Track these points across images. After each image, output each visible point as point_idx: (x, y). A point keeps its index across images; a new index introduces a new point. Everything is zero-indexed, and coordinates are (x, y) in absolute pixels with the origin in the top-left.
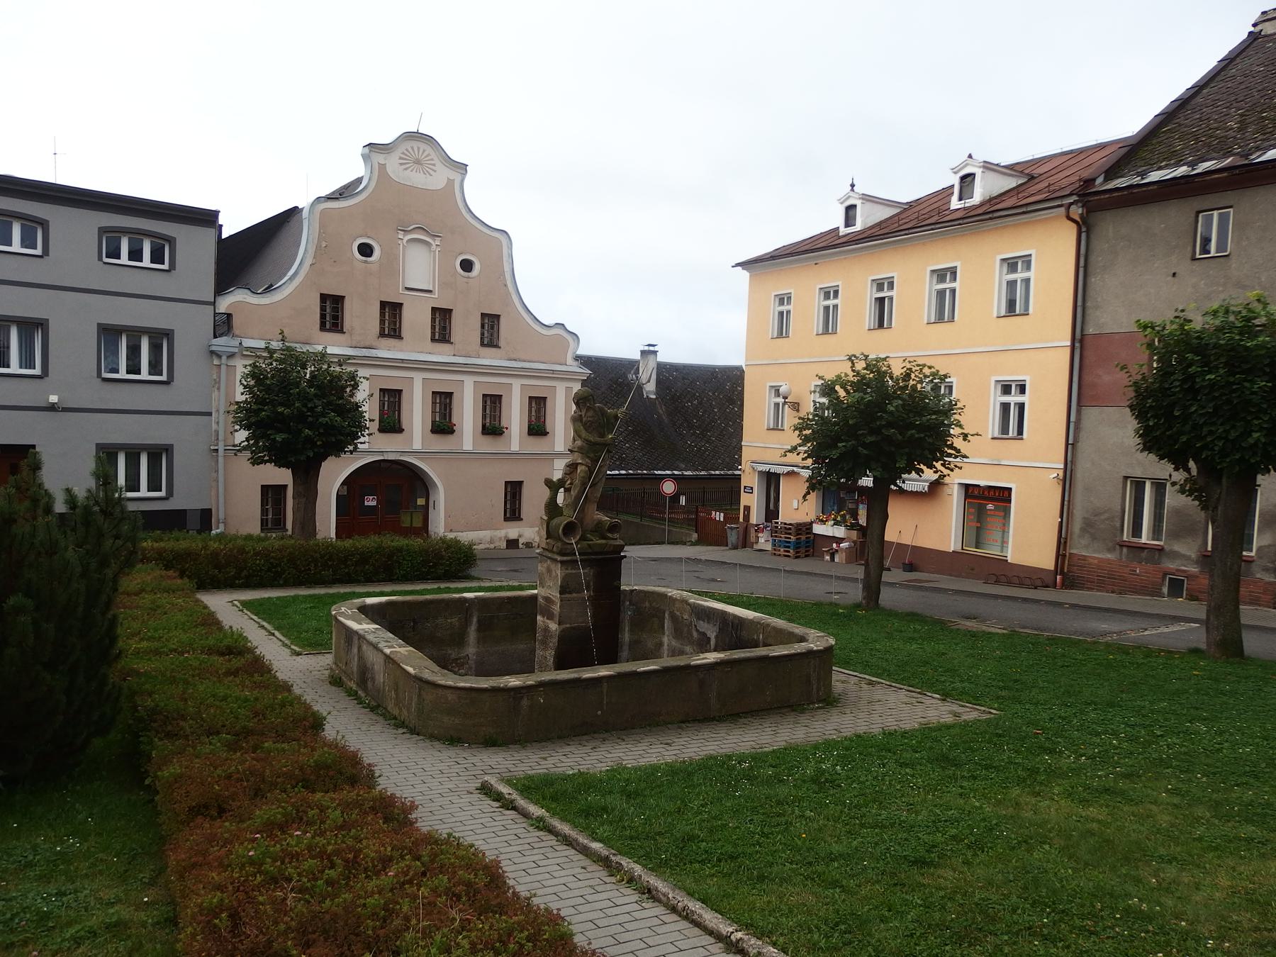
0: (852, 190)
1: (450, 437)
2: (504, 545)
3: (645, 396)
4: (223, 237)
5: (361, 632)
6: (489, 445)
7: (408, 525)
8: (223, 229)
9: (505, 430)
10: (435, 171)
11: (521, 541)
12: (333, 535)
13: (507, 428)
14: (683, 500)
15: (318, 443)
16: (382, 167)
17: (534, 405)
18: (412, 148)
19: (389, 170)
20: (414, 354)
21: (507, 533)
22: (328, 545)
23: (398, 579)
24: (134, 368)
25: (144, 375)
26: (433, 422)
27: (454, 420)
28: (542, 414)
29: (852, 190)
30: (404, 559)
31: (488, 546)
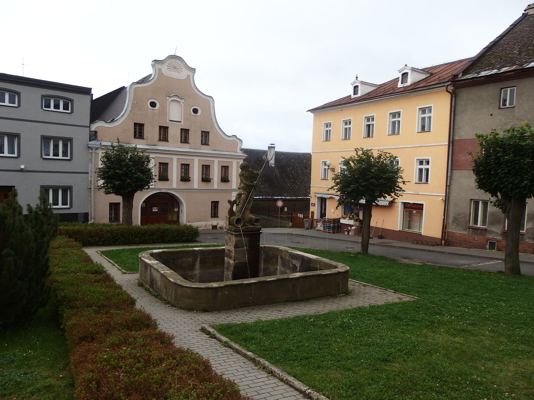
0: (357, 79)
1: (188, 183)
2: (211, 228)
3: (270, 166)
4: (93, 99)
5: (151, 264)
6: (205, 186)
7: (171, 220)
8: (93, 96)
9: (211, 180)
10: (182, 72)
11: (218, 226)
12: (139, 224)
13: (212, 179)
14: (286, 209)
15: (133, 185)
16: (160, 70)
17: (223, 169)
18: (173, 62)
19: (163, 71)
20: (173, 148)
21: (212, 223)
22: (137, 228)
23: (166, 242)
24: (56, 154)
25: (60, 157)
26: (181, 176)
27: (190, 176)
28: (227, 173)
29: (357, 79)
30: (169, 234)
31: (204, 228)
